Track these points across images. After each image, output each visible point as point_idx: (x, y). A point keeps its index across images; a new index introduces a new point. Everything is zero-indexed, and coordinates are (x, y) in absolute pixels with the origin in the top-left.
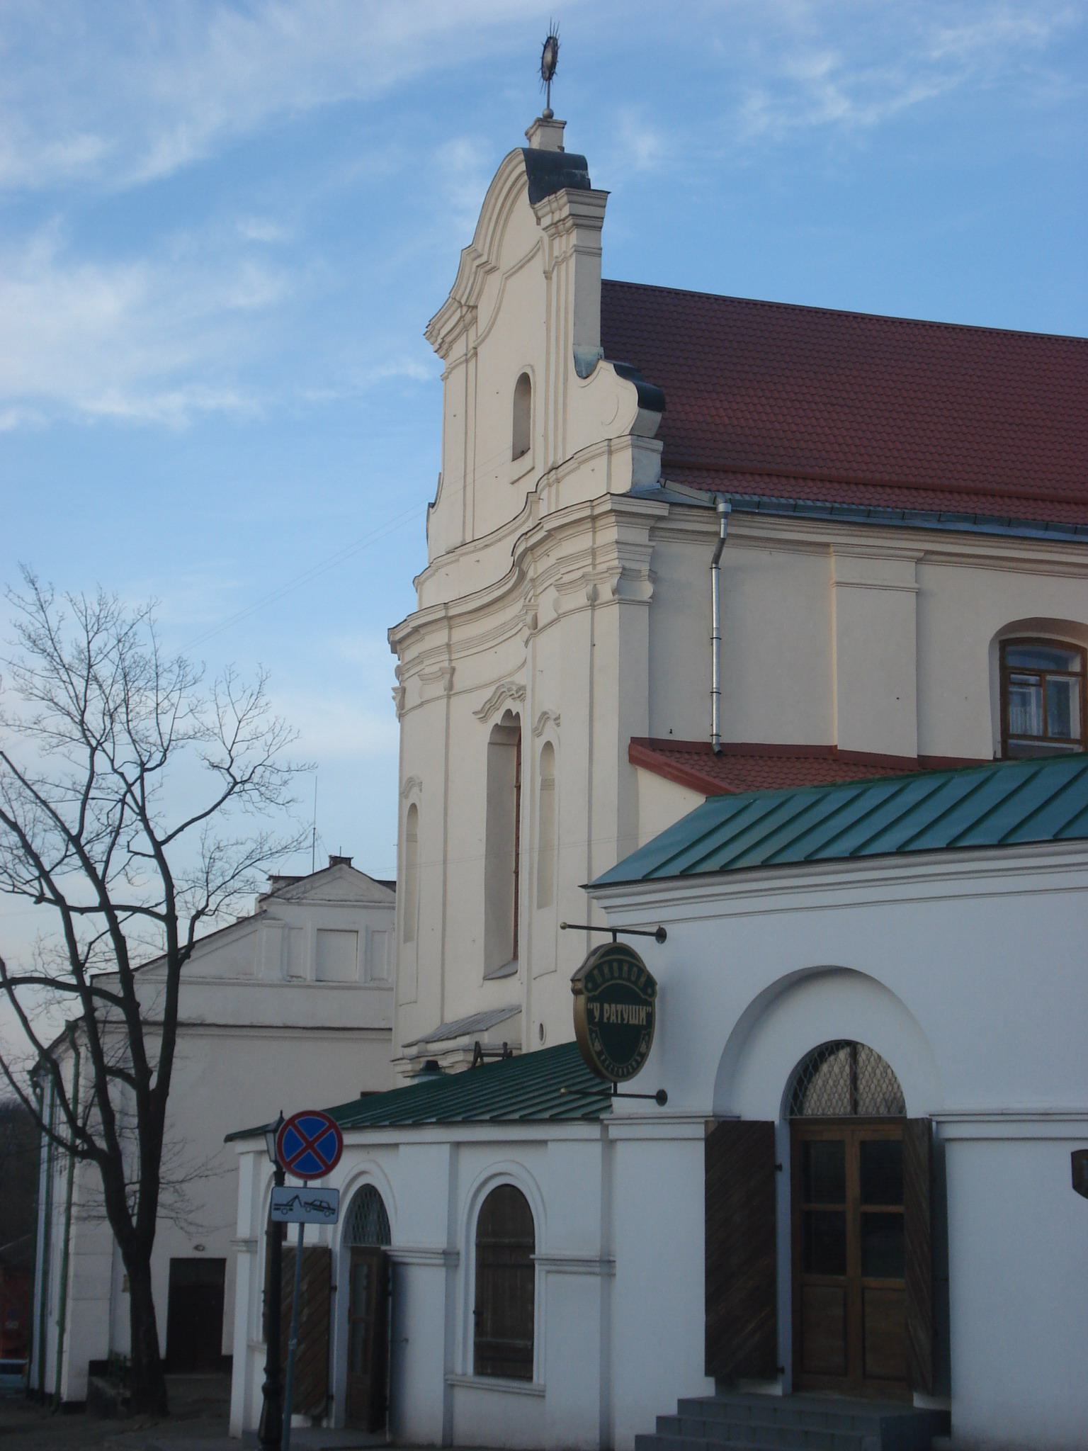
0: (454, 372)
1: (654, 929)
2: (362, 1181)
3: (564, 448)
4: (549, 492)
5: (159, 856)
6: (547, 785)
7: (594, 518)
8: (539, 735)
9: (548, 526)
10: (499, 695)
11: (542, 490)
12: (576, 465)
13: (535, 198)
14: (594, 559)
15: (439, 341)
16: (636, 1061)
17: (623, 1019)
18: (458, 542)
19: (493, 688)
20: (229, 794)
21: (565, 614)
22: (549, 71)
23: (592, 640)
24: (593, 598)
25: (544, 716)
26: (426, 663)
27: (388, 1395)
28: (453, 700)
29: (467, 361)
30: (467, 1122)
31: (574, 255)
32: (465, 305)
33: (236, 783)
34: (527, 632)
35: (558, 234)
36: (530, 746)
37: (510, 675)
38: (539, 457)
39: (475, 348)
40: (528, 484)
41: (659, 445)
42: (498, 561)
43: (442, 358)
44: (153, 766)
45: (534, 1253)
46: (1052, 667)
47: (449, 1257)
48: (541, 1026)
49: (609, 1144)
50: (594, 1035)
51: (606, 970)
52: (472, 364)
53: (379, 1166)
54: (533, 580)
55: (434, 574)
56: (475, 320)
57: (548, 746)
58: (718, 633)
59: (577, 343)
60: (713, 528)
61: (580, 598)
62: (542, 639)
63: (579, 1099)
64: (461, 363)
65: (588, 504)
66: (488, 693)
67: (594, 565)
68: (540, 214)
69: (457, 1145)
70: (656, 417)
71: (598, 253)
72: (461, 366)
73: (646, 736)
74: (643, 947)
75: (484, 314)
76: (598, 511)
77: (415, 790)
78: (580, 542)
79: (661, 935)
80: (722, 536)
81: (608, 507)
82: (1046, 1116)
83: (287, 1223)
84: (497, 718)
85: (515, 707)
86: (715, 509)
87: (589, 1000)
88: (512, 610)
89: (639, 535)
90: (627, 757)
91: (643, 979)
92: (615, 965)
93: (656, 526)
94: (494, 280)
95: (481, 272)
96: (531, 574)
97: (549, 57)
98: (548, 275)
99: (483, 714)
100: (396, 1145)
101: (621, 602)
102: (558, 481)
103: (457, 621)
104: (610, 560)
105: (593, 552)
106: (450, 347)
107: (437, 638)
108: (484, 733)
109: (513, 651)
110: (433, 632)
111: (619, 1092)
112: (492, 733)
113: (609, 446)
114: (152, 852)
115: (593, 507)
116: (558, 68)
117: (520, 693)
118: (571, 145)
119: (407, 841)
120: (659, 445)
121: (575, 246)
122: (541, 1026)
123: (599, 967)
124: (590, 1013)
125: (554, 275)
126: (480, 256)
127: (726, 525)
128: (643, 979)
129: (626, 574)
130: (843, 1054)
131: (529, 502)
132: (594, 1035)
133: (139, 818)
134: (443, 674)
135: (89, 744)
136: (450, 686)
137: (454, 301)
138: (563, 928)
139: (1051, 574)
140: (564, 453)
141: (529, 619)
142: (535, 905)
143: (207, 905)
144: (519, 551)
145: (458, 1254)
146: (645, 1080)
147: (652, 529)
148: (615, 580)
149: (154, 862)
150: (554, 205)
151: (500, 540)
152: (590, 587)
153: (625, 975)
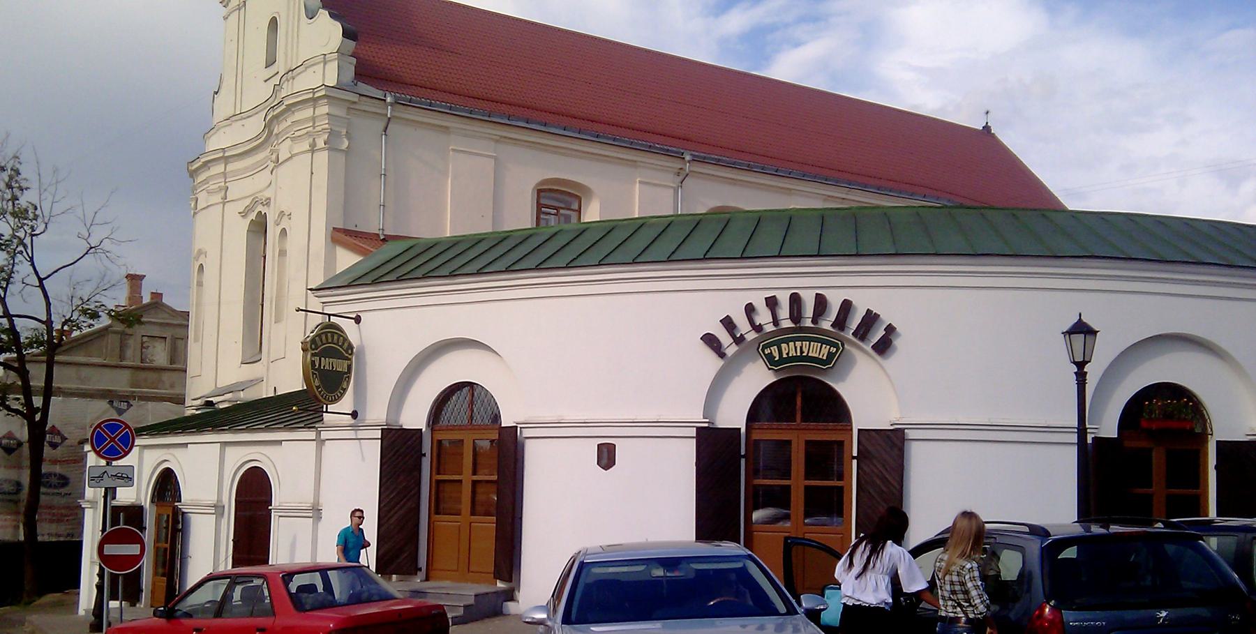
1: (354, 316)
3: (297, 59)
4: (288, 85)
5: (42, 286)
6: (283, 253)
10: (255, 202)
12: (304, 69)
14: (314, 123)
16: (340, 392)
17: (802, 352)
18: (232, 113)
20: (86, 253)
21: (297, 154)
24: (313, 145)
26: (211, 183)
27: (180, 520)
28: (227, 205)
29: (239, 9)
33: (91, 248)
34: (272, 165)
36: (273, 232)
38: (281, 66)
40: (276, 80)
42: (255, 126)
43: (224, 6)
44: (39, 232)
46: (563, 206)
47: (218, 509)
48: (275, 388)
49: (321, 442)
51: (324, 338)
53: (174, 456)
54: (277, 135)
55: (216, 133)
58: (385, 171)
60: (384, 112)
62: (282, 170)
64: (235, 10)
65: (311, 91)
66: (248, 202)
69: (225, 444)
72: (235, 12)
73: (342, 227)
74: (347, 326)
76: (317, 95)
77: (203, 256)
79: (358, 320)
80: (389, 116)
81: (323, 93)
82: (585, 424)
84: (253, 216)
85: (264, 210)
86: (385, 100)
87: (313, 355)
88: (261, 156)
89: (340, 112)
91: (346, 345)
92: (329, 334)
93: (351, 107)
96: (275, 131)
99: (244, 215)
104: (323, 124)
105: (314, 119)
107: (218, 169)
108: (244, 224)
110: (215, 165)
111: (329, 410)
113: (325, 58)
114: (38, 284)
115: (314, 93)
117: (267, 203)
119: (197, 285)
122: (275, 388)
123: (319, 335)
124: (313, 363)
127: (392, 110)
128: (346, 345)
129: (333, 134)
130: (466, 390)
132: (315, 376)
133: (30, 263)
134: (220, 190)
138: (297, 311)
139: (563, 154)
140: (292, 89)
141: (274, 157)
142: (273, 322)
146: (346, 403)
149: (39, 290)
151: (256, 113)
152: (311, 140)
153: (335, 341)
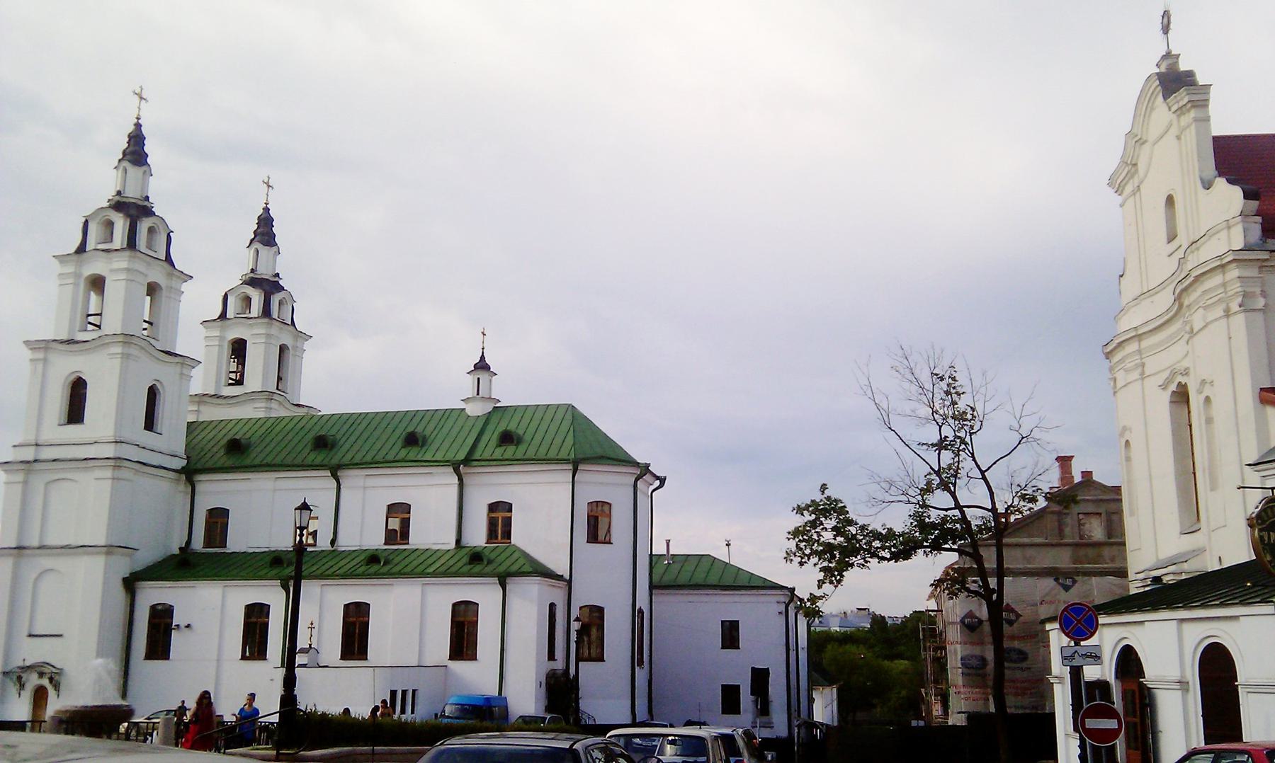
0: (1128, 201)
2: (1125, 643)
5: (984, 478)
6: (1209, 421)
7: (1222, 266)
8: (1201, 393)
9: (1195, 273)
10: (1174, 374)
11: (1188, 255)
13: (1165, 98)
14: (1225, 289)
15: (1117, 186)
19: (1168, 371)
22: (1166, 29)
23: (1229, 334)
24: (1228, 314)
25: (1203, 382)
26: (1127, 361)
29: (1134, 194)
30: (1186, 607)
31: (1193, 127)
32: (1131, 163)
33: (1023, 438)
34: (1187, 336)
35: (1183, 114)
36: (1195, 400)
37: (1178, 362)
38: (1183, 239)
39: (1139, 186)
40: (1180, 254)
41: (1259, 219)
42: (1165, 300)
45: (1237, 681)
50: (1266, 551)
51: (1269, 513)
52: (1138, 195)
54: (1188, 306)
56: (1136, 171)
57: (1207, 399)
59: (1201, 171)
61: (1219, 311)
62: (1196, 339)
63: (1263, 589)
66: (1166, 375)
67: (1225, 292)
68: (1170, 105)
69: (1183, 620)
70: (1254, 204)
71: (1207, 119)
75: (1142, 167)
77: (1127, 432)
78: (1217, 279)
83: (1082, 666)
84: (1173, 387)
85: (1183, 380)
87: (1260, 530)
89: (1252, 272)
90: (1258, 400)
94: (1147, 147)
95: (1138, 144)
96: (1186, 303)
97: (1166, 20)
98: (1178, 138)
99: (1164, 387)
100: (1142, 622)
101: (1245, 311)
102: (1198, 249)
103: (1144, 336)
104: (1236, 287)
105: (1224, 285)
106: (1124, 189)
107: (1132, 347)
108: (1166, 396)
109: (1179, 349)
112: (1171, 396)
113: (1228, 224)
116: (1172, 26)
117: (1186, 373)
118: (1183, 66)
120: (1259, 219)
121: (1193, 118)
124: (1261, 538)
125: (1183, 137)
126: (1136, 136)
131: (1181, 264)
135: (938, 425)
136: (1143, 373)
137: (1124, 162)
141: (1188, 328)
142: (1208, 488)
143: (1013, 502)
144: (1177, 292)
145: (1188, 683)
147: (1260, 267)
148: (1240, 299)
150: (1179, 98)
